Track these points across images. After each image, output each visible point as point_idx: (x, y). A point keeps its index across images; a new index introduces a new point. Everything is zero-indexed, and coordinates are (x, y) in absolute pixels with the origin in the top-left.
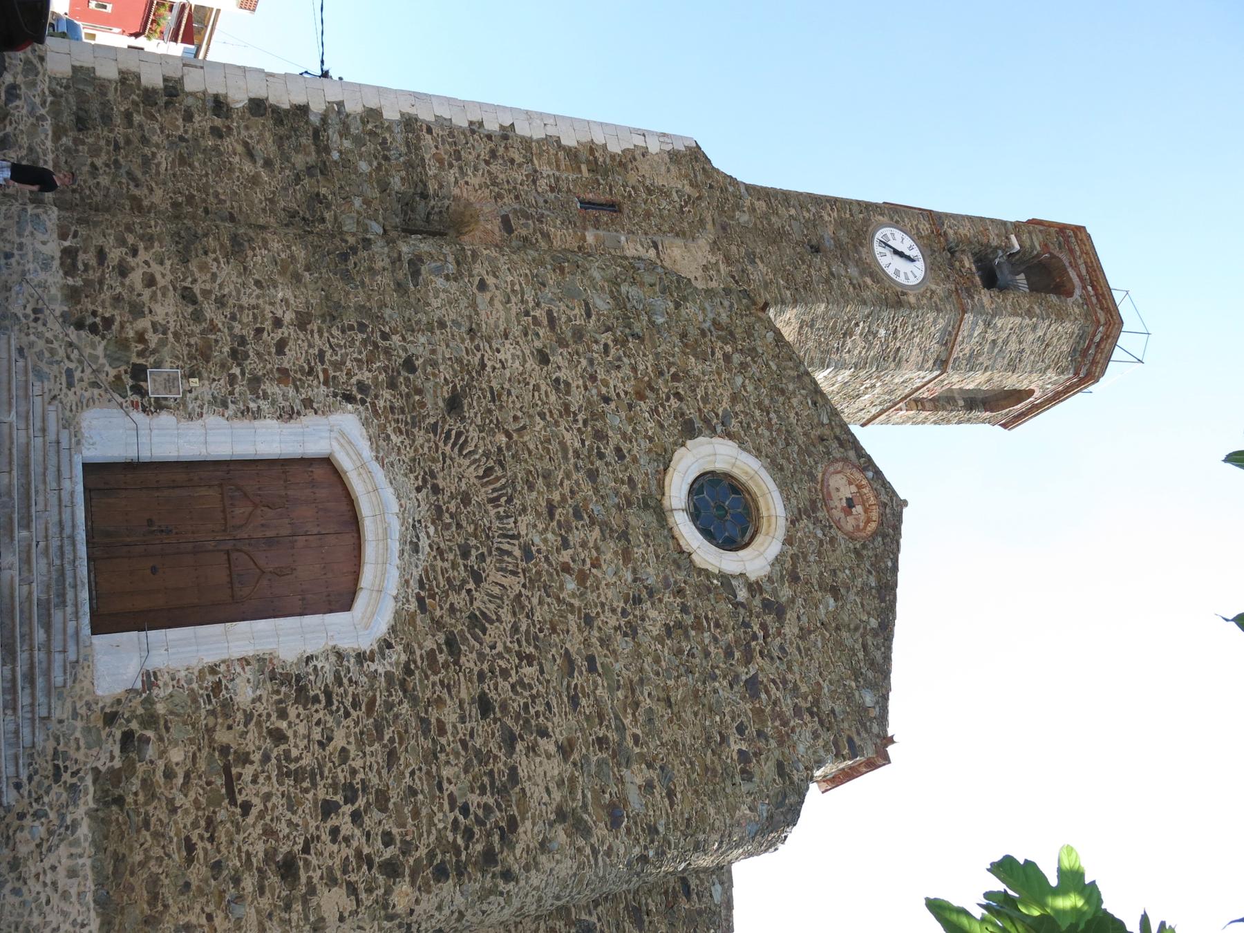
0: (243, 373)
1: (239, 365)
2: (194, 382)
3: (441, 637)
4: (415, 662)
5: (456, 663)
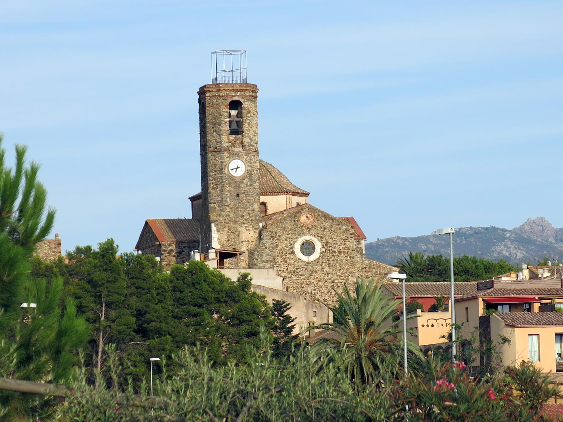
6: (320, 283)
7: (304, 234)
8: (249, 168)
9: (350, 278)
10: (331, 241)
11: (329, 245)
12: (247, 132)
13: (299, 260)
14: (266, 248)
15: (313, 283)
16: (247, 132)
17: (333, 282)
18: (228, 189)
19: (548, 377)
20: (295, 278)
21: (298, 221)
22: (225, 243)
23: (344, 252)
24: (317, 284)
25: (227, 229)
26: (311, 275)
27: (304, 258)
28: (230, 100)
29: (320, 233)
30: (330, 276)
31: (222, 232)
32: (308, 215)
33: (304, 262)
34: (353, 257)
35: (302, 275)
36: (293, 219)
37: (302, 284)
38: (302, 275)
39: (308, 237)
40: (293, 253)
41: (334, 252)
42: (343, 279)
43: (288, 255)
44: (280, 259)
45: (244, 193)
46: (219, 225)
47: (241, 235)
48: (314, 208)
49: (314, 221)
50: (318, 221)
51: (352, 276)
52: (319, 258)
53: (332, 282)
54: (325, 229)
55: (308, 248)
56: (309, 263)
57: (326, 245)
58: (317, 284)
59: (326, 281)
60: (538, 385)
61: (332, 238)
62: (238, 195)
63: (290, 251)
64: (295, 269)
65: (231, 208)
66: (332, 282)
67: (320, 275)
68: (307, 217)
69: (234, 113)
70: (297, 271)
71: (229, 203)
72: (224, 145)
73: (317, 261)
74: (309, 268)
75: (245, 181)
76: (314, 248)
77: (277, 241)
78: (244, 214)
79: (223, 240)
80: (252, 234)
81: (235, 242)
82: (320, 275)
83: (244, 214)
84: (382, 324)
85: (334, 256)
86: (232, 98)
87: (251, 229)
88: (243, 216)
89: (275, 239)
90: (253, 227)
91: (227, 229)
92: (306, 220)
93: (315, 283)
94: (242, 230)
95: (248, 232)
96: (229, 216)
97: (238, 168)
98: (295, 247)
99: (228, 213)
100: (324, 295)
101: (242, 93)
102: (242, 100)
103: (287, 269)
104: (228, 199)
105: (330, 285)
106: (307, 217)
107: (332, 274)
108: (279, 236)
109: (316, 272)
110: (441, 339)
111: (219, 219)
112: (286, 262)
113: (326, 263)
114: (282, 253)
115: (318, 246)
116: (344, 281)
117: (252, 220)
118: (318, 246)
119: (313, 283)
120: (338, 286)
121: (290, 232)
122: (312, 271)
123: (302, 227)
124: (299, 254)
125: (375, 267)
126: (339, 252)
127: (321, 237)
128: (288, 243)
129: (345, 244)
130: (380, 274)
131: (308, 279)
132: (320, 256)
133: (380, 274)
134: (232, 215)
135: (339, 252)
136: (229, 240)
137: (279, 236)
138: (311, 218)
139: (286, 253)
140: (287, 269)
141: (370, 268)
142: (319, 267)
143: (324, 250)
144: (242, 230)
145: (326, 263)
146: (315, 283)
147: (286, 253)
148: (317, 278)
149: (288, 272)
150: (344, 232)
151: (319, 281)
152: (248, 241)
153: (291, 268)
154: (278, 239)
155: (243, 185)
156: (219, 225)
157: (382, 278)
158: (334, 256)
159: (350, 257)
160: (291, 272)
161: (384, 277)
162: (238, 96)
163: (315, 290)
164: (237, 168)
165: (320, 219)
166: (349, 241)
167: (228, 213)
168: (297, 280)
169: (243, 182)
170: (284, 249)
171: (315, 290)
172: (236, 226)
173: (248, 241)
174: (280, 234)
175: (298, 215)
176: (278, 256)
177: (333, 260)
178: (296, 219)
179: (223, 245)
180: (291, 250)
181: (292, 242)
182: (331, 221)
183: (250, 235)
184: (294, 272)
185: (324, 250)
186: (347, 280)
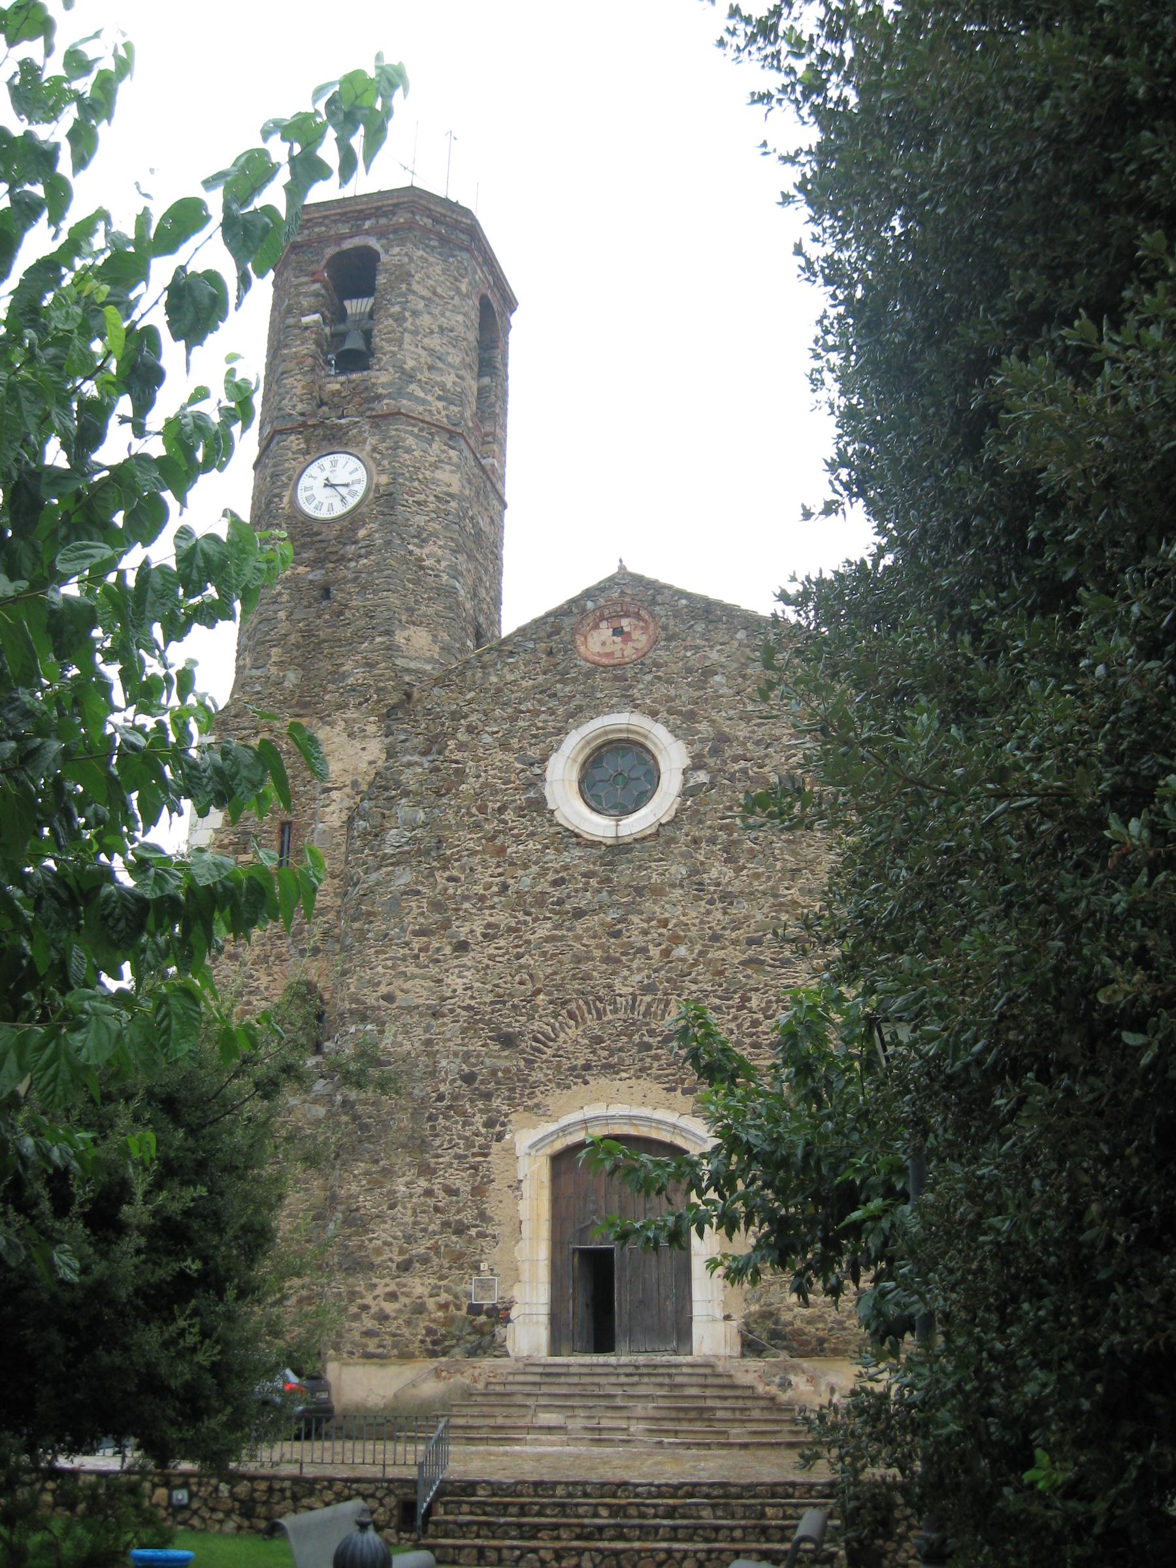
6: (681, 951)
8: (384, 479)
15: (644, 950)
16: (388, 348)
19: (171, 812)
24: (666, 953)
27: (598, 826)
29: (686, 694)
30: (741, 909)
32: (625, 622)
33: (594, 844)
35: (579, 914)
37: (578, 960)
40: (539, 805)
43: (509, 815)
44: (470, 840)
52: (675, 822)
53: (751, 942)
54: (708, 672)
56: (619, 849)
57: (715, 752)
58: (666, 953)
59: (715, 938)
60: (850, 969)
63: (521, 799)
66: (751, 942)
67: (676, 908)
68: (618, 631)
70: (557, 893)
73: (661, 834)
74: (624, 873)
76: (653, 776)
82: (676, 908)
89: (452, 744)
93: (654, 952)
97: (328, 485)
98: (548, 775)
101: (383, 221)
102: (374, 243)
103: (505, 887)
106: (618, 631)
110: (811, 224)
112: (502, 850)
113: (712, 841)
114: (482, 809)
115: (672, 757)
117: (378, 690)
119: (644, 950)
122: (639, 891)
127: (691, 716)
128: (510, 757)
131: (617, 934)
139: (502, 810)
140: (505, 887)
142: (679, 871)
143: (702, 777)
145: (712, 841)
146: (654, 952)
147: (502, 810)
148: (664, 923)
151: (676, 940)
154: (461, 746)
162: (367, 233)
163: (648, 989)
164: (333, 486)
170: (495, 792)
171: (648, 989)
176: (460, 825)
183: (367, 756)
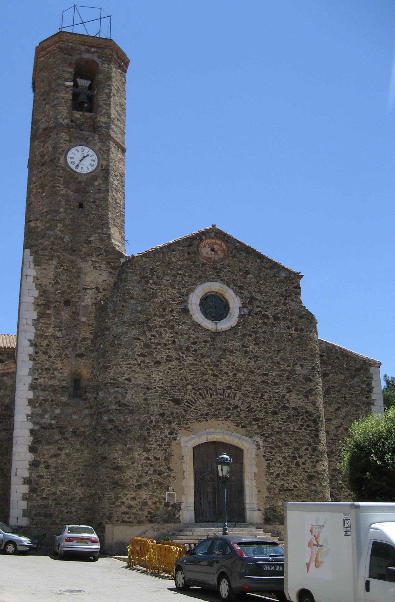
0: (167, 472)
1: (163, 473)
2: (170, 488)
3: (254, 423)
4: (261, 432)
5: (262, 419)
6: (240, 375)
7: (208, 279)
9: (298, 369)
10: (259, 297)
11: (256, 303)
12: (104, 107)
13: (197, 326)
14: (132, 298)
15: (226, 373)
17: (267, 375)
18: (63, 192)
20: (190, 360)
21: (197, 253)
22: (50, 288)
23: (285, 319)
24: (235, 375)
25: (54, 262)
26: (221, 357)
27: (208, 324)
28: (77, 57)
30: (260, 362)
31: (44, 266)
34: (302, 330)
35: (203, 356)
36: (186, 250)
37: (203, 374)
38: (203, 356)
39: (214, 286)
40: (186, 311)
41: (266, 317)
42: (285, 370)
43: (175, 314)
44: (159, 321)
45: (94, 202)
46: (41, 253)
47: (83, 276)
48: (225, 235)
49: (226, 256)
50: (234, 257)
51: (302, 365)
53: (264, 375)
54: (247, 273)
55: (215, 307)
56: (217, 334)
57: (250, 303)
58: (235, 375)
59: (252, 372)
61: (260, 292)
62: (81, 206)
63: (179, 308)
64: (189, 343)
65: (65, 226)
66: (264, 375)
67: (238, 359)
68: (213, 250)
69: (84, 83)
70: (194, 347)
71: (62, 215)
72: (61, 121)
73: (233, 330)
75: (96, 183)
77: (154, 287)
78: (92, 239)
79: (45, 281)
80: (105, 275)
81: (69, 287)
83: (92, 239)
84: (55, 592)
85: (265, 324)
86: (81, 54)
87: (104, 267)
88: (90, 242)
89: (151, 281)
90: (109, 263)
91: (54, 262)
92: (212, 255)
93: (231, 374)
94: (86, 266)
95: (98, 272)
96: (61, 239)
99: (59, 233)
100: (249, 400)
101: (99, 50)
102: (98, 61)
103: (174, 342)
104: (62, 210)
105: (260, 379)
106: (213, 250)
107: (263, 358)
108: (158, 277)
109: (231, 352)
111: (41, 244)
112: (172, 327)
114: (164, 310)
116: (287, 373)
118: (235, 303)
119: (226, 373)
120: (276, 384)
121: (180, 272)
123: (204, 264)
124: (198, 316)
125: (338, 355)
126: (276, 318)
127: (241, 288)
129: (285, 304)
130: (348, 369)
131: (217, 366)
132: (238, 323)
133: (348, 369)
134: (67, 238)
135: (276, 318)
136: (57, 283)
137: (158, 277)
138: (219, 253)
139: (172, 311)
140: (174, 342)
141: (329, 357)
144: (86, 266)
145: (250, 336)
146: (231, 374)
147: (172, 311)
148: (234, 364)
149: (175, 349)
150: (275, 306)
151: (238, 370)
152: (97, 288)
153: (181, 340)
154: (155, 283)
155: (91, 190)
156: (41, 253)
157: (353, 377)
158: (265, 324)
159: (296, 330)
160: (180, 349)
161: (356, 375)
163: (230, 388)
165: (237, 254)
166: (292, 300)
167: (59, 233)
168: (192, 364)
169: (93, 185)
170: (169, 304)
172: (74, 258)
173: (97, 288)
174: (160, 273)
175: (195, 242)
176: (155, 315)
177: (265, 332)
178: (191, 249)
179: (45, 292)
180: (183, 306)
181: (184, 291)
182: (258, 261)
183: (101, 279)
184: (188, 349)
185: (246, 311)
186: (293, 372)
